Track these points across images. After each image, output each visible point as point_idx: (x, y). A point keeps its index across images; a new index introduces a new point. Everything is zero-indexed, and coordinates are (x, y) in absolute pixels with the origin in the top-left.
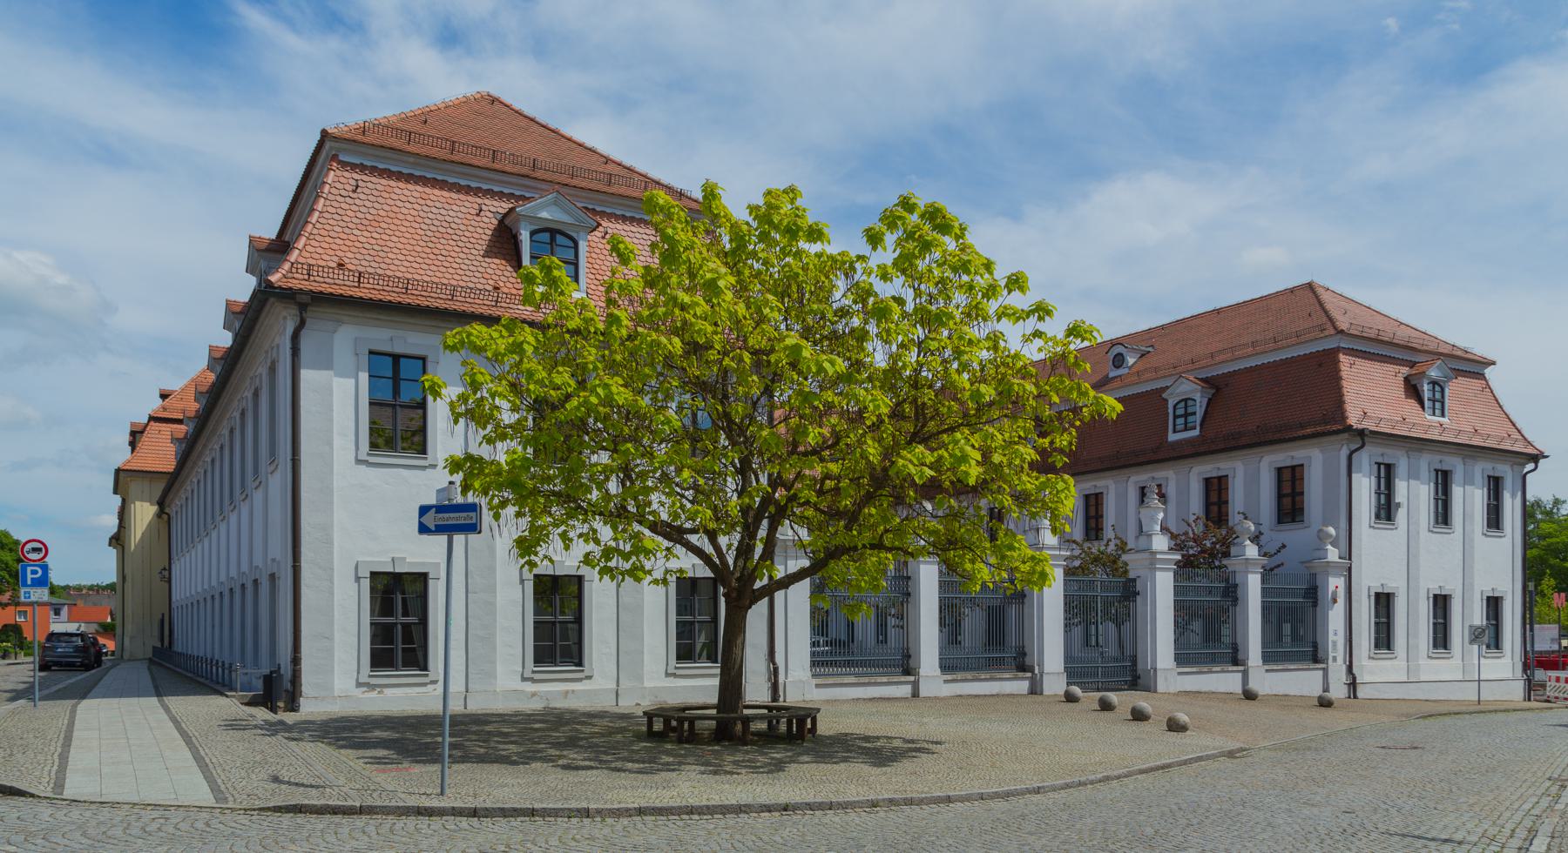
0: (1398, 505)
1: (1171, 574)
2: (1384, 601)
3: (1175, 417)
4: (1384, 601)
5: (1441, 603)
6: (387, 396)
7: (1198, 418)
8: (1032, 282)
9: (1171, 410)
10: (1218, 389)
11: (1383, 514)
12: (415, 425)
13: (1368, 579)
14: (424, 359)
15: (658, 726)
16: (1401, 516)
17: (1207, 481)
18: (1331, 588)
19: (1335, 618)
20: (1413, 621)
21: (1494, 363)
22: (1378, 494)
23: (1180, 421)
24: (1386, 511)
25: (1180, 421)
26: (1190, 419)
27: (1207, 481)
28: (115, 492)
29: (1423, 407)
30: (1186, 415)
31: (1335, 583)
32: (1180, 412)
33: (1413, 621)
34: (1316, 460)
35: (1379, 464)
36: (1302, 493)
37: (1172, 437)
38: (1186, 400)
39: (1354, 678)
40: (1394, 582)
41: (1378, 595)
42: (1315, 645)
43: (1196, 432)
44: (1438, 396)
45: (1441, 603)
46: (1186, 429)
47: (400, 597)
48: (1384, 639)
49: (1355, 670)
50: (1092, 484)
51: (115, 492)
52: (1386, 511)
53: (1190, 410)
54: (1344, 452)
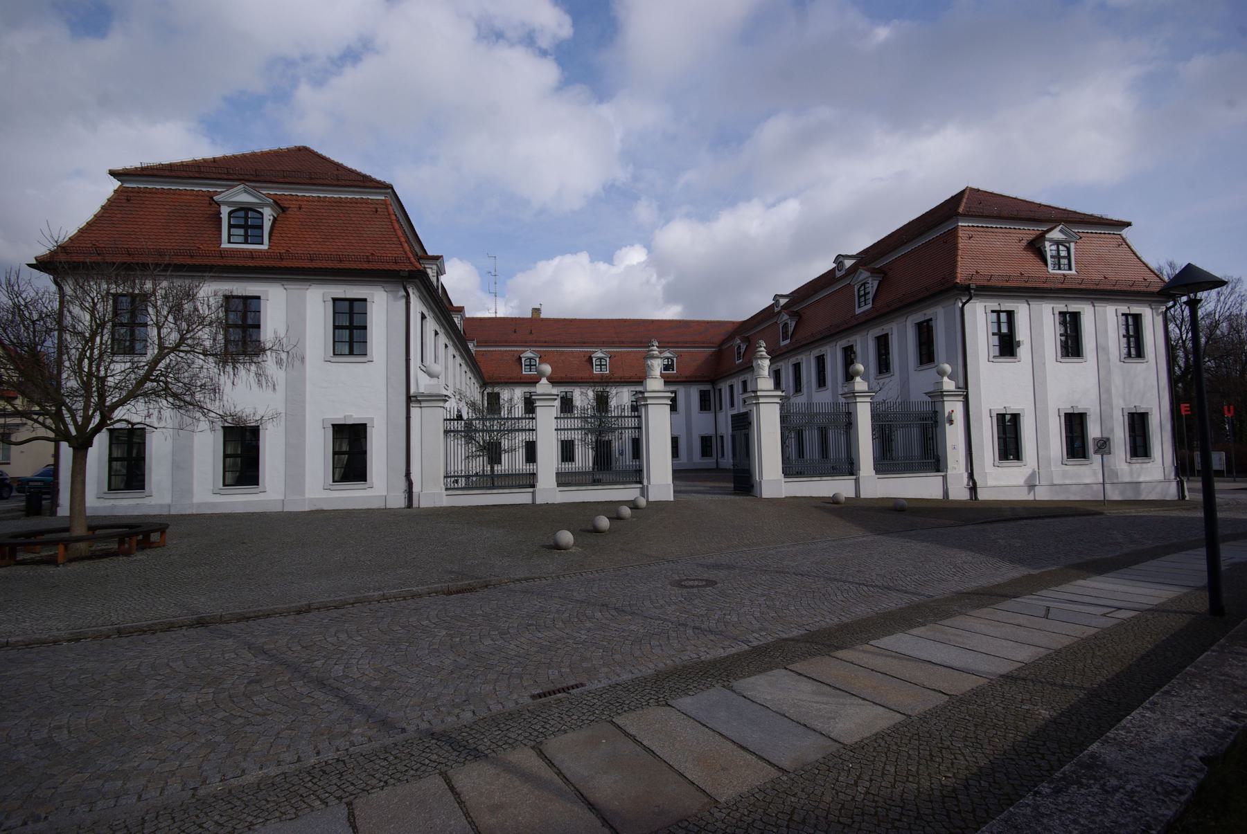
0: (1018, 344)
1: (778, 407)
3: (860, 297)
7: (870, 296)
11: (1133, 351)
12: (338, 345)
15: (155, 537)
16: (1023, 351)
18: (947, 409)
19: (954, 436)
21: (1129, 224)
22: (1127, 336)
24: (1007, 346)
29: (1046, 265)
30: (866, 294)
31: (953, 407)
34: (939, 315)
35: (998, 312)
36: (258, 326)
37: (858, 311)
39: (974, 483)
41: (1001, 417)
42: (938, 460)
44: (1063, 253)
49: (976, 477)
52: (1007, 346)
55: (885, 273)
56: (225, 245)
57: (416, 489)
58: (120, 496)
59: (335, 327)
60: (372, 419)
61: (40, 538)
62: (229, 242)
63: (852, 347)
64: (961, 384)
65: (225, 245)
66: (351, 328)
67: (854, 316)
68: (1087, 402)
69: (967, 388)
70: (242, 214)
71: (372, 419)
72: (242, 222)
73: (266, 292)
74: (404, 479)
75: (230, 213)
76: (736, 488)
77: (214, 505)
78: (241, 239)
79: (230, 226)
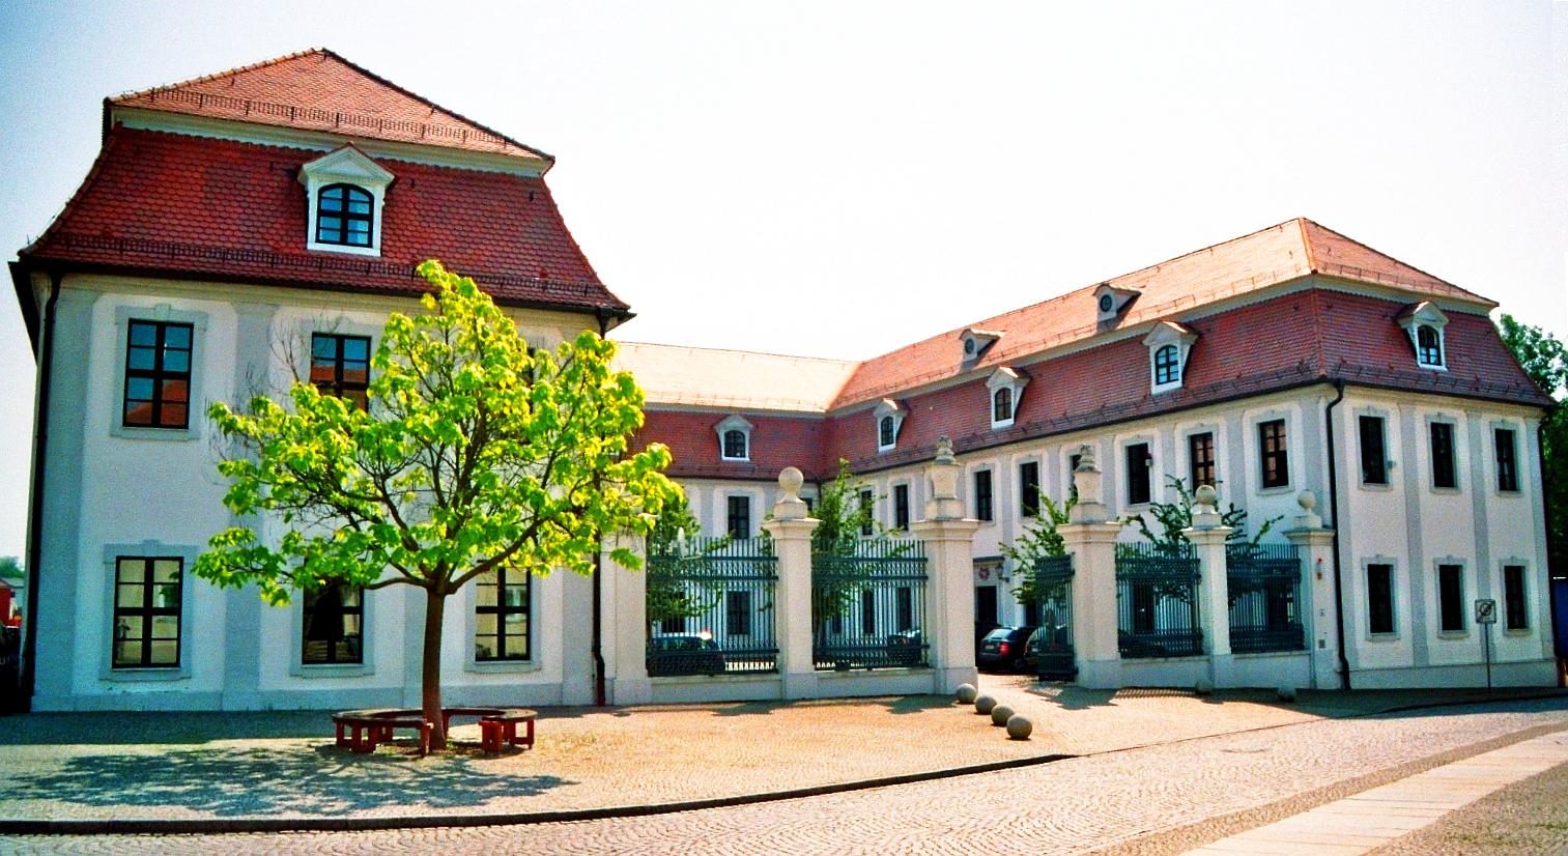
2: (1380, 578)
3: (1158, 367)
4: (1380, 578)
5: (1450, 578)
6: (147, 361)
7: (1180, 367)
8: (153, 448)
9: (1153, 360)
10: (1201, 335)
13: (1358, 554)
14: (190, 326)
16: (1395, 476)
17: (1263, 427)
20: (1417, 600)
21: (1497, 304)
23: (1163, 371)
25: (1163, 371)
26: (1172, 369)
27: (1263, 427)
28: (324, 50)
30: (1168, 365)
32: (1162, 361)
33: (1417, 600)
37: (1156, 390)
38: (1167, 348)
40: (1393, 552)
43: (1178, 384)
45: (1450, 578)
46: (1169, 381)
47: (856, 594)
48: (1382, 619)
50: (974, 464)
51: (324, 50)
53: (1172, 359)
54: (1322, 406)
55: (1201, 335)
56: (312, 246)
57: (608, 674)
58: (138, 676)
59: (131, 373)
60: (1465, 560)
61: (399, 719)
62: (318, 241)
63: (1144, 447)
64: (1329, 522)
65: (312, 246)
66: (158, 374)
67: (1148, 396)
68: (1462, 551)
69: (1335, 525)
70: (338, 193)
71: (1500, 561)
72: (338, 207)
73: (205, 316)
74: (589, 654)
75: (321, 191)
76: (1040, 680)
77: (295, 695)
78: (336, 237)
79: (321, 213)
